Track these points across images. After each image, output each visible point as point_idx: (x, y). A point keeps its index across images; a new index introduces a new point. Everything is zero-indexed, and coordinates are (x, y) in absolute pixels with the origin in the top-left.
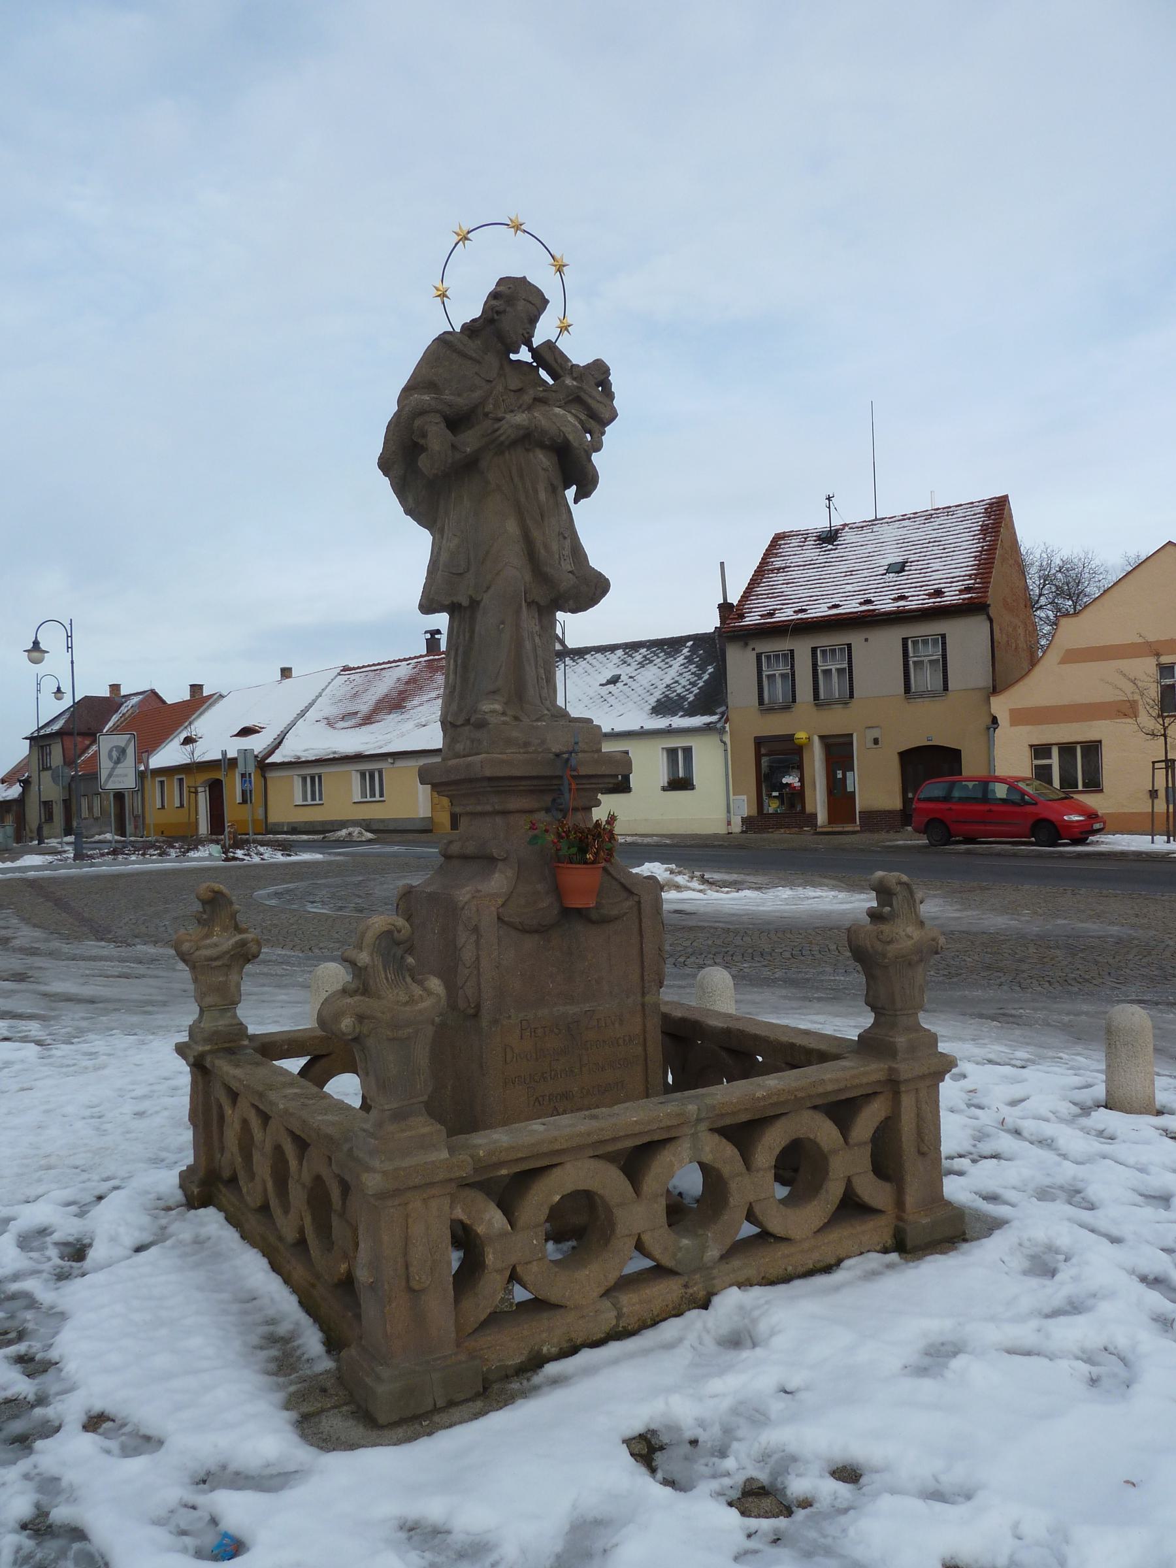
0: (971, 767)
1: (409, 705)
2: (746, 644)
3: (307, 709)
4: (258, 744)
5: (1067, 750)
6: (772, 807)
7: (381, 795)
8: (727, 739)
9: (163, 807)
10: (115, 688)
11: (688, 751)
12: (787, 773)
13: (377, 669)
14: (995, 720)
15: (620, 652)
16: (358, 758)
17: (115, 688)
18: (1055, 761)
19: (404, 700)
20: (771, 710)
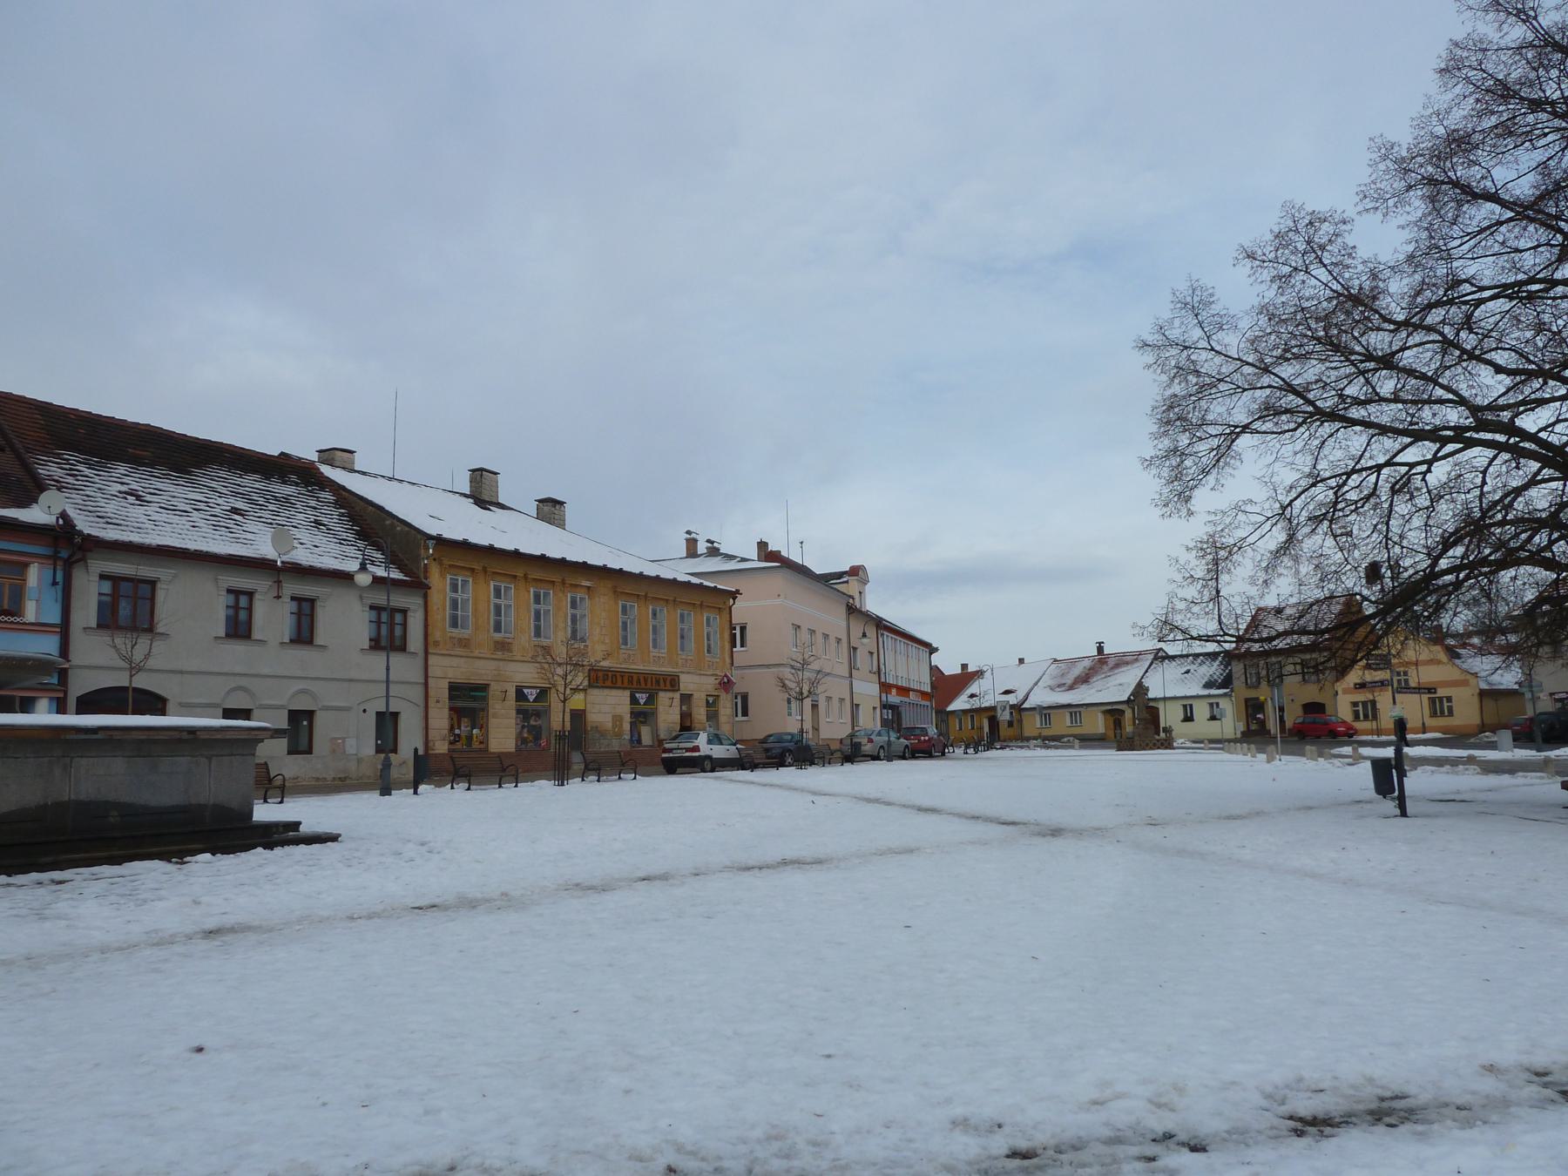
0: (1329, 710)
1: (1091, 681)
2: (1239, 660)
4: (1012, 699)
5: (1365, 704)
6: (1253, 727)
7: (1081, 723)
8: (1233, 699)
9: (961, 729)
10: (964, 666)
11: (1191, 706)
12: (1259, 713)
13: (1073, 662)
14: (1337, 692)
15: (1191, 658)
16: (1069, 706)
17: (964, 666)
18: (1360, 708)
19: (1089, 678)
20: (1250, 687)
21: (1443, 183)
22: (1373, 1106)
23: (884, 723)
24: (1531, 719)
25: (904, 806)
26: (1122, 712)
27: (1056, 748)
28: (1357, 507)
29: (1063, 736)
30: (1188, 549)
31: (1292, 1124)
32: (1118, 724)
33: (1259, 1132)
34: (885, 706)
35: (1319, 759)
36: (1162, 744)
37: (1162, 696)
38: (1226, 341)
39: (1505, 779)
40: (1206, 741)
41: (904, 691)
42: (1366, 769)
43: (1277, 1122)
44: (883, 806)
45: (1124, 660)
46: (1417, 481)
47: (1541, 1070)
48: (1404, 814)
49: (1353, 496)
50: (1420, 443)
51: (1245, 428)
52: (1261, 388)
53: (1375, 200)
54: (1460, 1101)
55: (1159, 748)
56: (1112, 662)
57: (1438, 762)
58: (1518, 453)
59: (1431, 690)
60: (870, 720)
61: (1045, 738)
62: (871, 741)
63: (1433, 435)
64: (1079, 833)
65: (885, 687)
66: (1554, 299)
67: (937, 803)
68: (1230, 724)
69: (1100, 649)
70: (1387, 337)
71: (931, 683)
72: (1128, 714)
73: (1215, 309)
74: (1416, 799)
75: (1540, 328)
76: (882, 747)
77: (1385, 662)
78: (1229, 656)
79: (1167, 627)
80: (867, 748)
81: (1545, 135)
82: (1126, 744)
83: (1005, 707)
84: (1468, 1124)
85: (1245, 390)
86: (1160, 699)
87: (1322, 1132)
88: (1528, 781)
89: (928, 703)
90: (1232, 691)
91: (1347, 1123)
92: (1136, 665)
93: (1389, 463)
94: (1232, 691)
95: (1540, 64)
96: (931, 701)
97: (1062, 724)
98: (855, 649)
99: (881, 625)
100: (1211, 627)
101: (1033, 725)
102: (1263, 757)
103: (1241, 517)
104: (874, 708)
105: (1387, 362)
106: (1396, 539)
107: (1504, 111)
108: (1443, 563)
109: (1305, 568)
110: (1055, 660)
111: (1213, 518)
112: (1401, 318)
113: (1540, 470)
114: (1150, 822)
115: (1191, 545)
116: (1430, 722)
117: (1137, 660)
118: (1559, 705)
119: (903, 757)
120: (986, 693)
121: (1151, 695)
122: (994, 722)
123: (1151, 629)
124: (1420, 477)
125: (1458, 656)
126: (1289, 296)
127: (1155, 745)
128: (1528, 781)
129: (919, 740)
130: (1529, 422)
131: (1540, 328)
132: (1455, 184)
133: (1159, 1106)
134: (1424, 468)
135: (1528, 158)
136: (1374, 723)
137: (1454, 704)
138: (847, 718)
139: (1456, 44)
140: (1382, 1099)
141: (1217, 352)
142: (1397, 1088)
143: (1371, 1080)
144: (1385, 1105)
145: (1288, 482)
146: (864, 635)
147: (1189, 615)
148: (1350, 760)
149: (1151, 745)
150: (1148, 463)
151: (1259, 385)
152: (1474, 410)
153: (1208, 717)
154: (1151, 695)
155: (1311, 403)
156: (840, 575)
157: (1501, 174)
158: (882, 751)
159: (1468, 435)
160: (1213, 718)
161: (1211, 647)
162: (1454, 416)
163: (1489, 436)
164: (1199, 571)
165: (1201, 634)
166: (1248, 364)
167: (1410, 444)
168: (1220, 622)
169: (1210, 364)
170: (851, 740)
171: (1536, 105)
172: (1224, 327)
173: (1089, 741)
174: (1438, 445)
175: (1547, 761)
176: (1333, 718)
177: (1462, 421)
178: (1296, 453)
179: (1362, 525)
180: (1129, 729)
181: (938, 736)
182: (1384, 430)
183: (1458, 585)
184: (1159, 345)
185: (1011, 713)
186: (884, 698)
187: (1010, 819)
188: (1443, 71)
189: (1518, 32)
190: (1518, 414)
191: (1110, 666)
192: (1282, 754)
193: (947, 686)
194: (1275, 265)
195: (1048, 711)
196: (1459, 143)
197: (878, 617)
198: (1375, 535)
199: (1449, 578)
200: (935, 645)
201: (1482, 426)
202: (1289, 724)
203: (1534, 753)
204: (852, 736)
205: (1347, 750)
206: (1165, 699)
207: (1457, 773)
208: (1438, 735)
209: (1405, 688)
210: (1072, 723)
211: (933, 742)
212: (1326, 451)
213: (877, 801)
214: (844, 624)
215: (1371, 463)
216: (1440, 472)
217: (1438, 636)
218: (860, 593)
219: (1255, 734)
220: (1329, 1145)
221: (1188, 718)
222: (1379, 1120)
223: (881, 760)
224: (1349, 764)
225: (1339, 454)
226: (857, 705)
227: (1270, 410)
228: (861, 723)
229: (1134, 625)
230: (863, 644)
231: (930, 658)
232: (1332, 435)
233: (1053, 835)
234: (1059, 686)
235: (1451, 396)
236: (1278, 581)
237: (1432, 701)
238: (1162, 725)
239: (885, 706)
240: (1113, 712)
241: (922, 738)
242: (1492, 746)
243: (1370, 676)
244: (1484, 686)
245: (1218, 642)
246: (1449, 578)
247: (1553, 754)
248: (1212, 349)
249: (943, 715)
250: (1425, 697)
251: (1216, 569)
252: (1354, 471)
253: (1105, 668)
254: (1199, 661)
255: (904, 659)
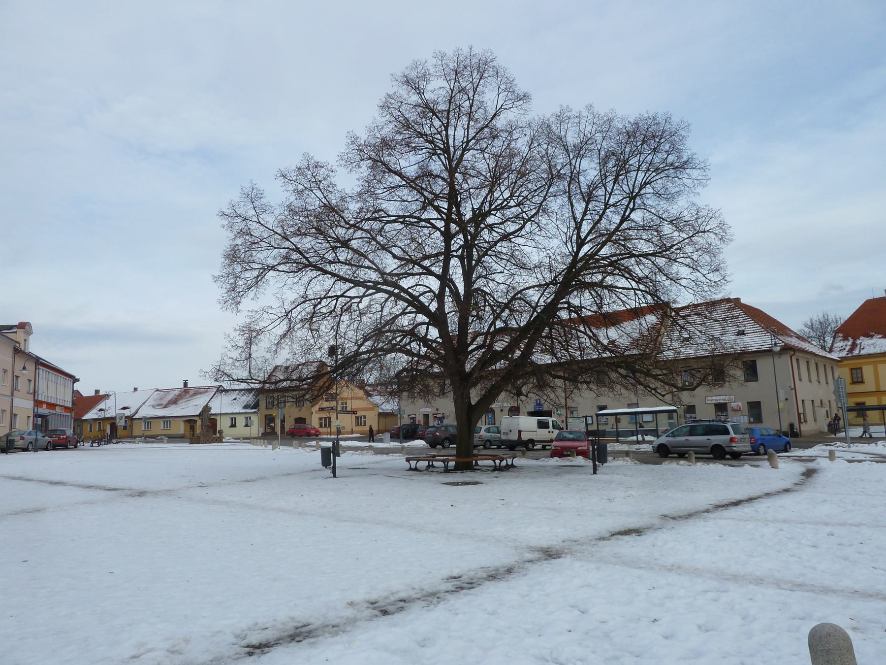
1: (179, 402)
3: (145, 402)
4: (127, 413)
5: (325, 419)
6: (268, 431)
10: (97, 391)
11: (235, 418)
13: (168, 391)
15: (238, 391)
16: (164, 417)
17: (97, 391)
18: (323, 421)
21: (378, 161)
22: (291, 633)
23: (35, 426)
24: (399, 427)
25: (40, 481)
26: (195, 421)
27: (153, 442)
28: (325, 316)
29: (158, 436)
30: (235, 330)
31: (247, 649)
32: (192, 428)
33: (229, 657)
34: (37, 416)
35: (300, 448)
36: (216, 440)
37: (219, 412)
38: (267, 219)
39: (384, 457)
40: (241, 439)
41: (52, 406)
42: (318, 454)
43: (239, 650)
44: (24, 482)
45: (199, 391)
46: (355, 306)
47: (373, 601)
48: (335, 476)
49: (324, 310)
50: (357, 287)
51: (273, 268)
52: (283, 248)
53: (349, 163)
54: (334, 623)
55: (214, 442)
56: (191, 392)
57: (356, 449)
58: (398, 297)
59: (354, 412)
60: (24, 425)
61: (146, 437)
62: (22, 438)
63: (363, 284)
64: (156, 493)
65: (38, 403)
66: (421, 227)
67: (64, 479)
68: (256, 428)
69: (185, 384)
70: (344, 231)
71: (73, 401)
72: (199, 422)
73: (263, 201)
74: (341, 468)
75: (413, 240)
76: (31, 442)
77: (334, 397)
78: (259, 392)
79: (220, 373)
80: (20, 443)
81: (422, 149)
82: (195, 439)
83: (122, 418)
84: (336, 634)
85: (275, 248)
86: (218, 414)
87: (263, 651)
88: (394, 458)
89: (69, 414)
90: (259, 410)
91: (277, 644)
92: (205, 395)
93: (342, 296)
94: (259, 410)
95: (423, 115)
96: (71, 413)
97: (158, 428)
98: (17, 377)
99: (39, 362)
100: (245, 374)
101: (140, 428)
102: (270, 447)
103: (265, 315)
104: (29, 417)
105: (345, 244)
106: (342, 334)
107: (407, 133)
108: (363, 349)
109: (296, 347)
110: (157, 390)
111: (250, 314)
112: (352, 222)
113: (407, 307)
114: (200, 485)
115: (238, 328)
116: (355, 428)
117: (207, 391)
118: (412, 421)
119: (46, 449)
120: (111, 408)
121: (212, 412)
122: (114, 427)
123: (210, 373)
124: (356, 304)
125: (370, 396)
126: (300, 203)
127: (212, 440)
128: (394, 458)
129: (59, 438)
130: (405, 283)
131: (413, 240)
132: (383, 163)
133: (173, 652)
134: (358, 300)
135: (414, 158)
136: (329, 429)
137: (367, 419)
138: (6, 423)
139: (389, 95)
140: (297, 628)
141: (261, 224)
142: (305, 621)
143: (293, 619)
144: (298, 631)
145: (293, 299)
146: (24, 368)
147: (233, 367)
148: (315, 448)
149: (210, 440)
150: (216, 279)
151: (283, 247)
152: (382, 273)
153: (244, 425)
154: (212, 412)
155: (307, 259)
156: (10, 327)
157: (403, 163)
158: (30, 445)
159: (379, 286)
160: (247, 425)
161: (243, 386)
162: (374, 276)
163: (389, 288)
164: (240, 343)
165: (239, 378)
166: (277, 233)
167: (353, 287)
168: (250, 372)
169: (257, 231)
170: (7, 437)
171: (421, 135)
172: (267, 212)
173: (174, 438)
174: (365, 289)
175: (403, 448)
176: (310, 426)
177: (377, 279)
178: (294, 284)
179: (325, 326)
180: (198, 430)
181: (73, 435)
182: (342, 279)
183: (369, 359)
184: (231, 216)
185: (126, 421)
186: (36, 411)
187: (113, 487)
188: (382, 107)
189: (414, 98)
190: (401, 279)
191: (191, 394)
192: (281, 445)
193: (82, 403)
194: (296, 183)
195: (169, 419)
196: (386, 144)
197: (37, 356)
198: (332, 331)
199: (365, 356)
200: (77, 377)
201: (386, 283)
202: (287, 429)
203: (399, 444)
204: (8, 435)
205: (314, 443)
206: (221, 414)
207: (363, 454)
208: (359, 435)
209: (344, 411)
210: (164, 427)
211: (69, 439)
212: (312, 285)
213: (20, 478)
214: (10, 360)
215: (334, 294)
216: (365, 301)
217: (362, 385)
218: (25, 340)
219: (269, 435)
220: (265, 658)
221: (233, 425)
222: (293, 640)
223: (29, 451)
224: (314, 451)
225: (319, 288)
226: (15, 415)
227: (286, 259)
228: (17, 426)
229: (201, 371)
230: (23, 374)
231: (73, 385)
232: (315, 277)
233: (139, 496)
234: (158, 405)
235: (374, 267)
236: (282, 351)
237: (357, 418)
238: (218, 429)
239: (37, 416)
240: (190, 422)
241: (62, 437)
242: (381, 441)
243: (326, 404)
244: (381, 411)
245: (248, 383)
246: (365, 356)
247: (406, 445)
248: (260, 223)
249: (79, 422)
250: (354, 416)
251: (250, 342)
252: (325, 297)
253: (188, 395)
254: (242, 393)
255: (54, 385)
